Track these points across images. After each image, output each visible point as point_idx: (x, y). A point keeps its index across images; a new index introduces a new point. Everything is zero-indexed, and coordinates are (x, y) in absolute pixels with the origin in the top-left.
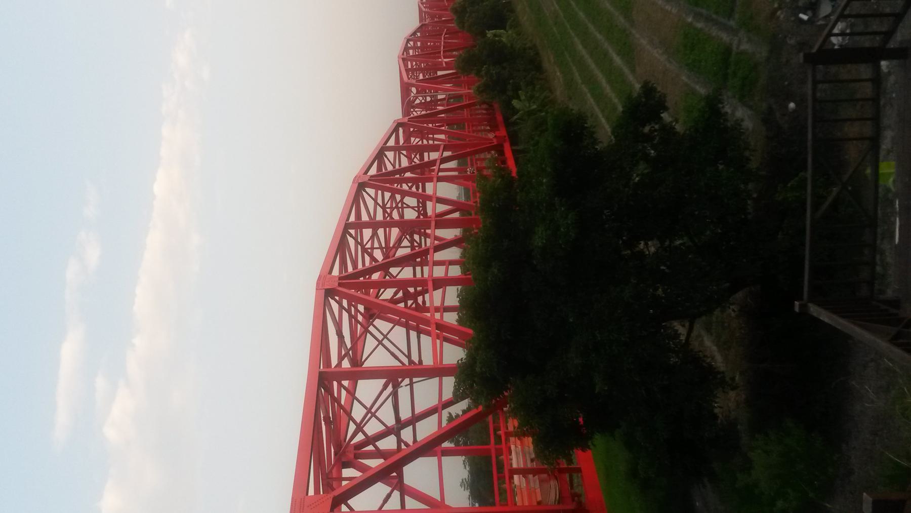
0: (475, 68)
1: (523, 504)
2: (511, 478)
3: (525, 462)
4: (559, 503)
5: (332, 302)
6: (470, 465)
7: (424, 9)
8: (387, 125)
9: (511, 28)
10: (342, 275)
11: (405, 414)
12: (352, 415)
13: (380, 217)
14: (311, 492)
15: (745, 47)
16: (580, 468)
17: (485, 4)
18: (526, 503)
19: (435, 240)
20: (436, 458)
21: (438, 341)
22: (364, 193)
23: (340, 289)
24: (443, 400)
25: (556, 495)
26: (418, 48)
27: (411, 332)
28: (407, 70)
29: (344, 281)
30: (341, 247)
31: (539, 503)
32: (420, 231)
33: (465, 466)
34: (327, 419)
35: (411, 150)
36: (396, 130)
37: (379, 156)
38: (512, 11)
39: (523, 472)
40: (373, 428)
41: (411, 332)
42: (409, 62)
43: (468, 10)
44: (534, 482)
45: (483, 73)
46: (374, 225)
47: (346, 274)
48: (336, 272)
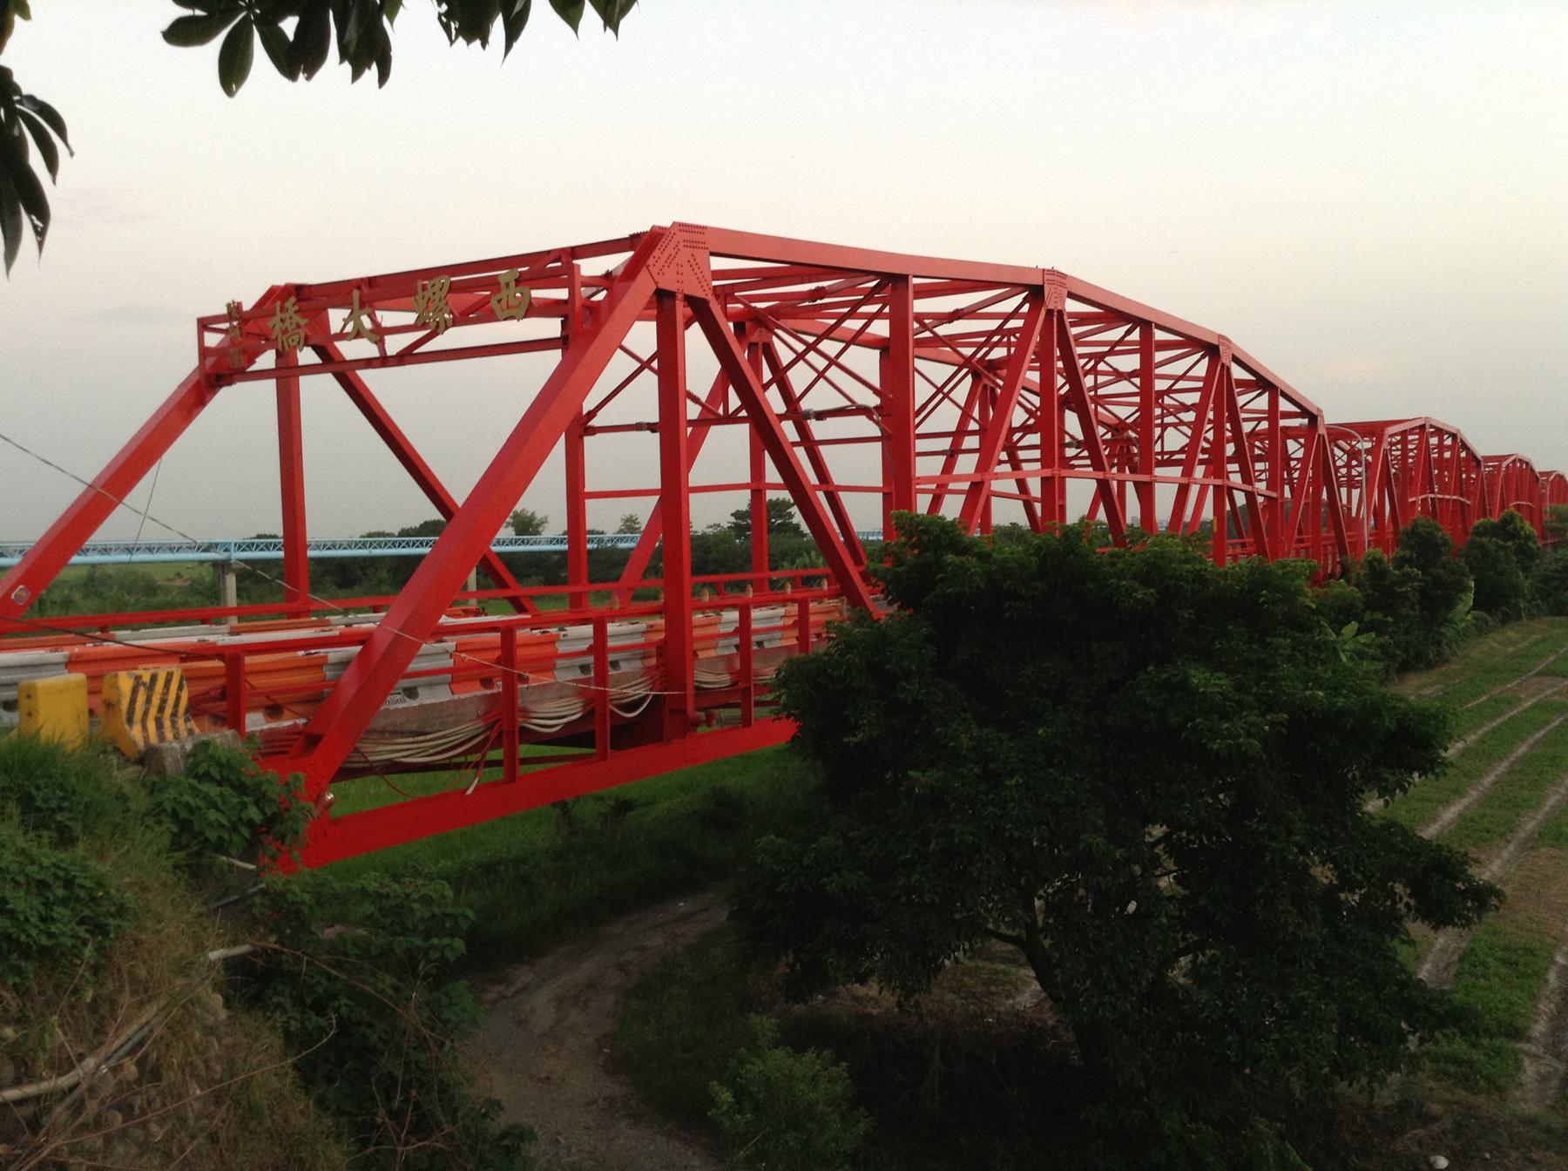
0: (1415, 555)
1: (695, 627)
2: (733, 606)
3: (758, 631)
4: (697, 688)
5: (1019, 299)
6: (715, 535)
7: (1504, 464)
8: (1313, 397)
9: (1474, 618)
10: (1065, 317)
11: (818, 429)
12: (825, 341)
13: (1160, 385)
14: (717, 264)
15: (1530, 1070)
16: (750, 725)
17: (1520, 573)
18: (696, 633)
19: (1202, 485)
20: (749, 480)
21: (933, 486)
22: (1198, 356)
23: (1043, 313)
24: (840, 493)
25: (705, 683)
26: (1441, 453)
27: (950, 440)
28: (1404, 434)
29: (1055, 319)
30: (1112, 315)
31: (695, 653)
32: (1115, 456)
33: (711, 527)
34: (820, 293)
35: (1276, 436)
36: (1305, 412)
37: (1262, 383)
38: (1505, 620)
39: (744, 628)
40: (799, 377)
41: (950, 440)
42: (1417, 437)
43: (1509, 543)
44: (728, 647)
45: (1407, 569)
46: (1146, 372)
47: (1068, 325)
48: (1072, 306)
